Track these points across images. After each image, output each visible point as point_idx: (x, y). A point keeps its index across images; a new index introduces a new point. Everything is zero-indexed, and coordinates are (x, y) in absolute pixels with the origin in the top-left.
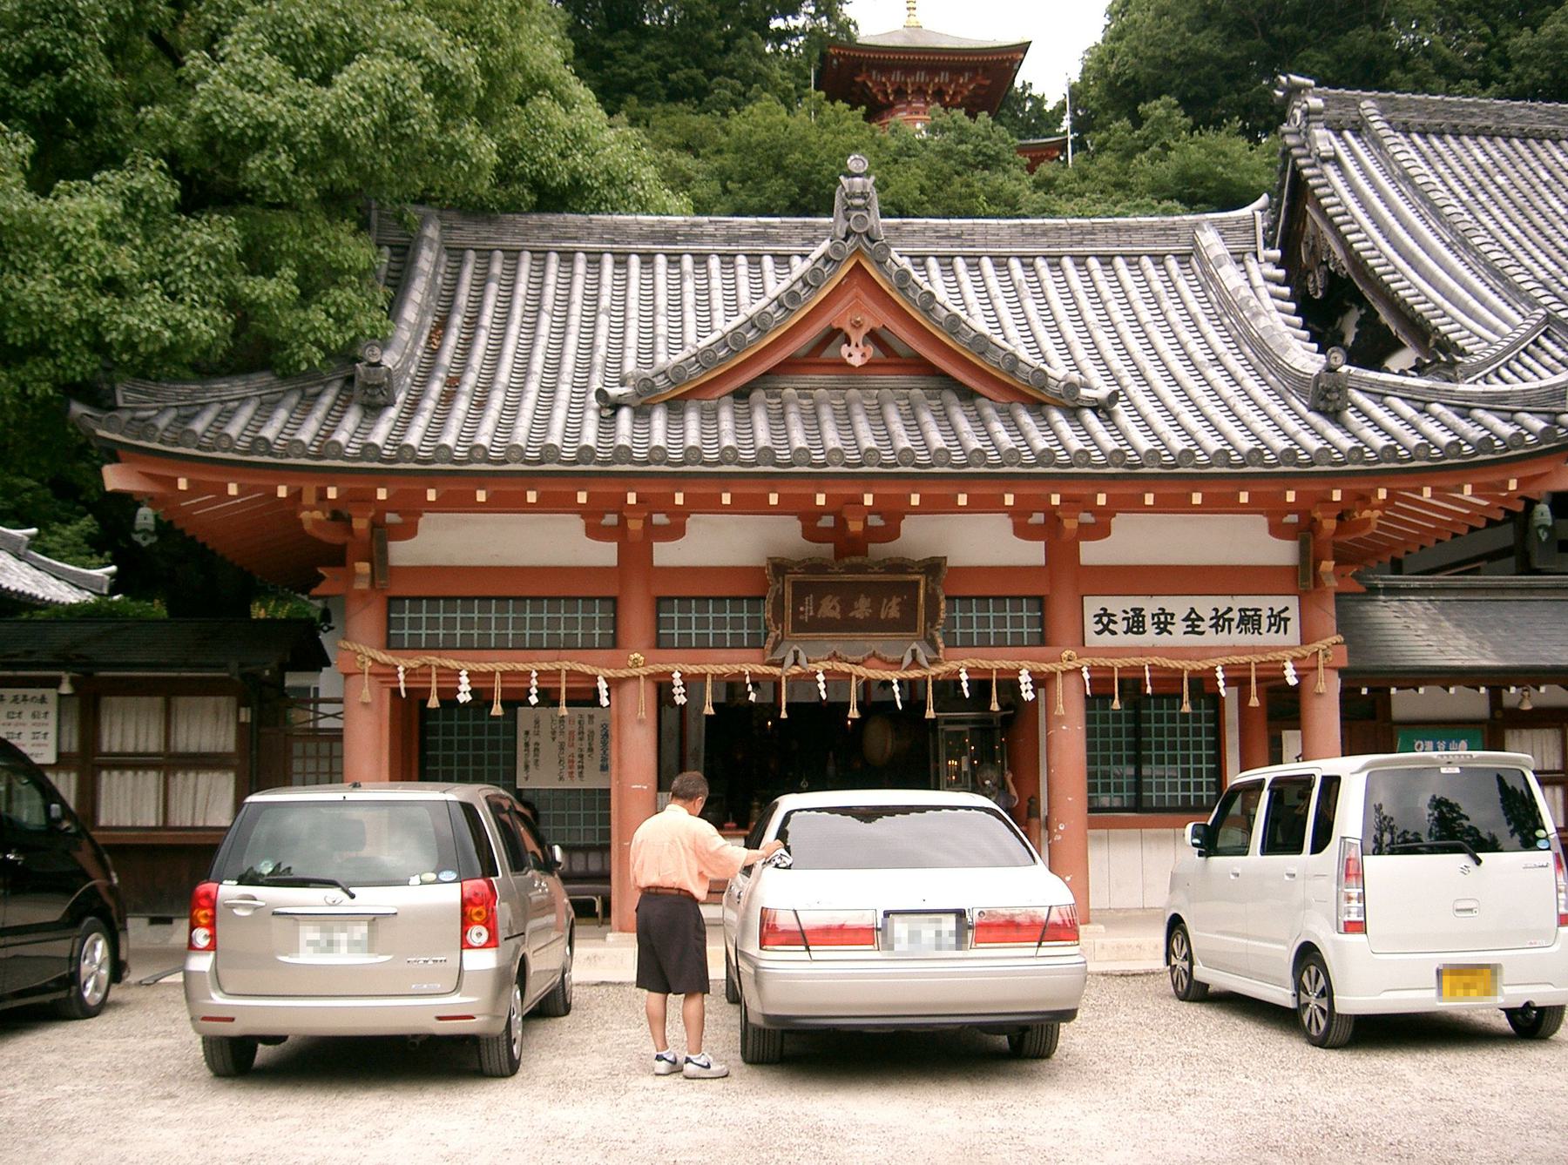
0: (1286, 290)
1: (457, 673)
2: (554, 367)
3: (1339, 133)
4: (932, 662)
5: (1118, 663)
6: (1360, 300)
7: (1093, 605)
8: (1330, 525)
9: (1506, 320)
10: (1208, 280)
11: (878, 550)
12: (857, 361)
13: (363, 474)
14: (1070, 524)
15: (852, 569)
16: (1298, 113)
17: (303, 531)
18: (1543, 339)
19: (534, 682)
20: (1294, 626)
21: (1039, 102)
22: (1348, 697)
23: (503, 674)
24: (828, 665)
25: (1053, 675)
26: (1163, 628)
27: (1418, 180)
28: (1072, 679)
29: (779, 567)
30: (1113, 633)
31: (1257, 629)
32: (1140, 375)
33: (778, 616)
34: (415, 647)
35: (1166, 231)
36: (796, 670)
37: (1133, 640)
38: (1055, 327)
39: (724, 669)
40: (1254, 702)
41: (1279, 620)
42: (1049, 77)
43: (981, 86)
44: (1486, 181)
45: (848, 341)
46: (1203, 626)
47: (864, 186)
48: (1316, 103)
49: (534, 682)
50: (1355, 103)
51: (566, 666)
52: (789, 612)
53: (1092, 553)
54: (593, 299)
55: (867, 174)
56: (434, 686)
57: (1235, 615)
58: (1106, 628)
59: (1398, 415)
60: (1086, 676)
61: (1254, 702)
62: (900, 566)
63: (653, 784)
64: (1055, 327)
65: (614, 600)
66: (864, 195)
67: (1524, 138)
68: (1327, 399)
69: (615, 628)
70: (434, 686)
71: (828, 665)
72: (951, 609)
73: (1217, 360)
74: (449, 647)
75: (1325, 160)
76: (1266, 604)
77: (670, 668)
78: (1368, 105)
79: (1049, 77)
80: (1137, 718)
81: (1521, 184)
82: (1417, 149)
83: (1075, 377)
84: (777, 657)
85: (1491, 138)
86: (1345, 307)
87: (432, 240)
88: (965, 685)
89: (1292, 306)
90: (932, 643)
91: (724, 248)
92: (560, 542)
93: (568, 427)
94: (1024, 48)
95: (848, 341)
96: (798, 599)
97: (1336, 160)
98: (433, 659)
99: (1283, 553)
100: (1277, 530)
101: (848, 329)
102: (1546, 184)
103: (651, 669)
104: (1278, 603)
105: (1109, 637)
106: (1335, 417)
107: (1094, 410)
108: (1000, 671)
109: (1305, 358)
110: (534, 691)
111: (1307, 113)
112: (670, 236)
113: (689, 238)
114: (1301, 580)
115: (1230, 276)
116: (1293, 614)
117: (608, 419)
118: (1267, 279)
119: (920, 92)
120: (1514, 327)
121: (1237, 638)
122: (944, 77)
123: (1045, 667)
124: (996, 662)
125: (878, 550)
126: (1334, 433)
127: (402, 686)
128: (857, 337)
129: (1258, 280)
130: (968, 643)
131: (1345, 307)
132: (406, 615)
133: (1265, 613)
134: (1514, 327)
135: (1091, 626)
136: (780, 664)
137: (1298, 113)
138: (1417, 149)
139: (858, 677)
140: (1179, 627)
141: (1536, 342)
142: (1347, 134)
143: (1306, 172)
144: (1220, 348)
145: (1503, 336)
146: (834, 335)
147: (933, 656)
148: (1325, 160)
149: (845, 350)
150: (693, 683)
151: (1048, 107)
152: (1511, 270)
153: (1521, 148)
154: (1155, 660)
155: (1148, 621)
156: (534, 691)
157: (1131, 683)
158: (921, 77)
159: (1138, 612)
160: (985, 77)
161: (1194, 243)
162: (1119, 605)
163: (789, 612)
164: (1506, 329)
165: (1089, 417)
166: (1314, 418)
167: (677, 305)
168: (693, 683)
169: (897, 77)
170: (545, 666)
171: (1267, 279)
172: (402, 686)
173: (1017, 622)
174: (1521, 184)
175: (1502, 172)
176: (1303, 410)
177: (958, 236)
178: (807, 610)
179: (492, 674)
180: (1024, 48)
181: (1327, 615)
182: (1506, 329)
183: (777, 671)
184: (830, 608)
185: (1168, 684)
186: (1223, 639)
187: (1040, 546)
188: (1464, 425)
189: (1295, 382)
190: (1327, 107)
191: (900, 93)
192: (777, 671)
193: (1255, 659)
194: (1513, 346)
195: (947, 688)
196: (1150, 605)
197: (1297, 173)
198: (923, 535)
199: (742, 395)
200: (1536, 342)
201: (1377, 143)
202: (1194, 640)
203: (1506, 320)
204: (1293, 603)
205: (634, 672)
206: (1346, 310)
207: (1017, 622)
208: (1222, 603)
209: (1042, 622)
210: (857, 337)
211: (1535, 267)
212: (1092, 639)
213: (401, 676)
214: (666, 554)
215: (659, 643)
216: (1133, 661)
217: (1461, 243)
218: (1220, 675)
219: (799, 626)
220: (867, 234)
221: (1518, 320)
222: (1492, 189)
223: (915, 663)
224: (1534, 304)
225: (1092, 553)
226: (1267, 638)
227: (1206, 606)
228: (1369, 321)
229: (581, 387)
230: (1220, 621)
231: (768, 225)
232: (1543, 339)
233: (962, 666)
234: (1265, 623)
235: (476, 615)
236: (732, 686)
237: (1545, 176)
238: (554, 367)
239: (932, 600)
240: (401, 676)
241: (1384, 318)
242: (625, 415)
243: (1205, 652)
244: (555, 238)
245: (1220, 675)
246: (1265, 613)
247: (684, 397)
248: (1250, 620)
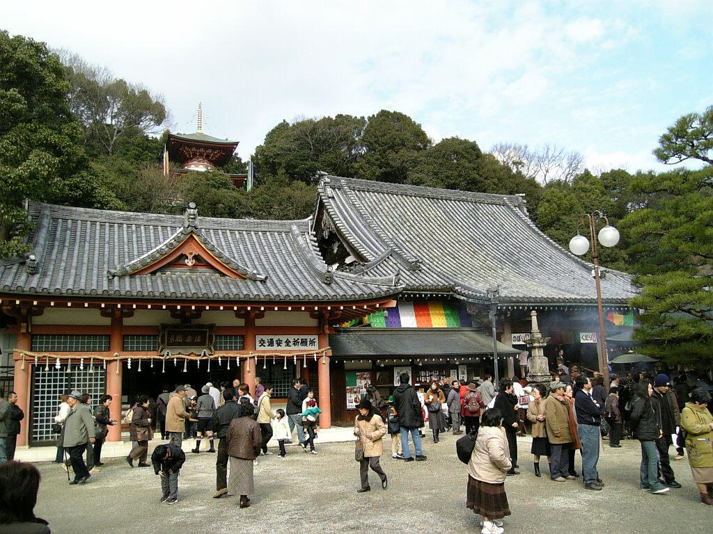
0: (317, 244)
1: (55, 359)
2: (90, 261)
3: (334, 189)
4: (210, 355)
5: (266, 355)
6: (339, 240)
7: (258, 338)
8: (327, 315)
9: (380, 251)
10: (294, 241)
11: (195, 322)
12: (190, 264)
13: (27, 297)
14: (253, 314)
15: (187, 327)
16: (322, 182)
17: (4, 314)
18: (390, 257)
19: (82, 362)
20: (317, 344)
21: (240, 160)
22: (332, 364)
23: (72, 359)
24: (178, 356)
25: (246, 359)
26: (279, 345)
27: (357, 206)
28: (252, 360)
29: (164, 326)
30: (264, 346)
31: (306, 345)
32: (274, 270)
33: (163, 342)
34: (40, 351)
35: (282, 225)
36: (168, 357)
37: (270, 348)
38: (248, 254)
39: (145, 357)
40: (305, 366)
41: (312, 342)
42: (245, 153)
43: (221, 155)
44: (376, 207)
45: (187, 258)
46: (291, 344)
47: (194, 212)
48: (328, 180)
49: (82, 362)
50: (339, 180)
51: (92, 356)
52: (166, 340)
53: (258, 322)
54: (102, 238)
55: (195, 208)
56: (47, 364)
57: (300, 341)
58: (262, 345)
59: (347, 285)
60: (256, 359)
61: (305, 366)
62: (202, 326)
63: (121, 394)
64: (248, 254)
65: (109, 336)
66: (194, 215)
67: (388, 194)
68: (329, 280)
69: (109, 344)
70: (47, 364)
71: (178, 356)
72: (216, 339)
73: (296, 266)
74: (53, 350)
75: (330, 198)
76: (309, 338)
77: (127, 357)
78: (343, 181)
79: (245, 153)
80: (270, 371)
81: (386, 208)
82: (357, 196)
83: (255, 272)
84: (162, 354)
85: (378, 193)
86: (333, 246)
87: (47, 216)
88: (220, 362)
89: (317, 244)
90: (210, 350)
91: (146, 223)
92: (93, 317)
93: (97, 283)
94: (236, 144)
95: (187, 258)
96: (169, 336)
97: (333, 198)
98: (47, 354)
99: (313, 323)
100: (312, 316)
101: (188, 255)
102: (393, 208)
103: (121, 357)
104: (312, 337)
105: (264, 348)
106: (329, 285)
107: (261, 281)
108: (231, 357)
109: (321, 265)
110: (82, 365)
111: (325, 183)
112: (129, 219)
113: (135, 219)
114: (318, 330)
115: (300, 240)
116: (316, 340)
117: (110, 281)
118: (311, 240)
119: (201, 155)
120: (382, 253)
121: (300, 347)
122: (210, 151)
123: (244, 356)
124: (231, 354)
125: (195, 322)
126: (329, 290)
127: (36, 363)
128: (190, 257)
129: (308, 241)
130: (221, 350)
131: (333, 246)
132: (38, 340)
133: (308, 340)
134: (382, 253)
135: (258, 344)
136: (163, 356)
137: (322, 182)
138: (357, 196)
139: (187, 359)
140: (284, 344)
141: (388, 258)
142: (337, 190)
143: (324, 201)
144: (297, 262)
145: (379, 256)
146: (184, 257)
147: (210, 353)
148: (330, 198)
149: (186, 261)
150: (135, 362)
151: (243, 162)
152: (382, 235)
153: (387, 197)
154: (277, 354)
155: (275, 342)
156: (82, 365)
157: (269, 360)
158: (202, 150)
159: (272, 340)
160: (222, 154)
161: (290, 229)
162: (266, 338)
163: (166, 340)
164: (380, 253)
165: (259, 283)
166: (323, 285)
167: (130, 241)
168: (135, 362)
169: (194, 149)
170: (86, 357)
171: (311, 240)
172: (36, 363)
173: (236, 343)
174: (386, 208)
175: (381, 204)
176: (320, 282)
177: (220, 223)
178: (172, 340)
179: (68, 359)
180: (236, 144)
181: (326, 341)
182: (380, 253)
183: (161, 358)
184: (179, 339)
185: (280, 360)
186: (296, 348)
187: (243, 320)
188: (365, 289)
189: (320, 274)
190: (331, 181)
191: (194, 155)
192: (161, 358)
193: (305, 353)
194: (382, 259)
195: (214, 362)
196: (275, 338)
197: (321, 201)
198: (209, 317)
199: (153, 273)
200: (388, 258)
201: (345, 193)
202: (288, 348)
203: (380, 251)
204: (316, 337)
205: (116, 358)
206: (334, 242)
207: (236, 343)
208: (296, 337)
209: (243, 343)
210: (190, 257)
211: (389, 234)
212: (258, 348)
213: (36, 360)
214: (127, 321)
215: (124, 349)
216: (271, 354)
217: (368, 226)
218: (295, 358)
219: (169, 344)
220: (195, 227)
221: (384, 251)
222: (378, 209)
223: (205, 355)
224: (388, 246)
225: (258, 322)
226: (309, 347)
227: (291, 338)
228: (341, 246)
229: (100, 269)
230: (296, 343)
231: (160, 217)
232: (390, 257)
233: (219, 355)
234: (308, 343)
235: (62, 340)
236: (146, 363)
237: (394, 206)
238: (90, 261)
239: (211, 337)
240: (36, 360)
241: (345, 246)
242: (116, 278)
243: (290, 351)
244: (90, 217)
245: (295, 358)
246: (308, 340)
247: (135, 274)
248: (304, 342)
